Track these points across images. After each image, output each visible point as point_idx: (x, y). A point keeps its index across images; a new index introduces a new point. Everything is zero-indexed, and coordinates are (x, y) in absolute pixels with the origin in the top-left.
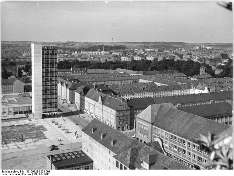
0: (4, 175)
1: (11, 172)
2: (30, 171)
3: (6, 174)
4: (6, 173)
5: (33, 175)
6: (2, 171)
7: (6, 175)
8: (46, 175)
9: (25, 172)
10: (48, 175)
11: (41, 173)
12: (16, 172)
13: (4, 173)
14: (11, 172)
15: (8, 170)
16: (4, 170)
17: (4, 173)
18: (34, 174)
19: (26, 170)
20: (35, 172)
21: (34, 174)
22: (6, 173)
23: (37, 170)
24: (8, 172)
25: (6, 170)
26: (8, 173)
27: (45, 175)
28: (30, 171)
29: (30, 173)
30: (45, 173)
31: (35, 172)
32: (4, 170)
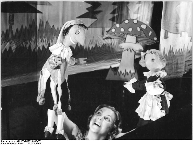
0: (4, 144)
3: (5, 144)
4: (5, 143)
5: (28, 144)
6: (2, 141)
8: (38, 144)
9: (20, 141)
10: (39, 144)
11: (34, 143)
12: (13, 142)
14: (9, 142)
17: (3, 143)
18: (28, 143)
19: (22, 140)
20: (29, 141)
21: (28, 143)
22: (5, 143)
23: (30, 140)
24: (7, 141)
27: (37, 144)
29: (25, 142)
31: (29, 141)
32: (3, 140)
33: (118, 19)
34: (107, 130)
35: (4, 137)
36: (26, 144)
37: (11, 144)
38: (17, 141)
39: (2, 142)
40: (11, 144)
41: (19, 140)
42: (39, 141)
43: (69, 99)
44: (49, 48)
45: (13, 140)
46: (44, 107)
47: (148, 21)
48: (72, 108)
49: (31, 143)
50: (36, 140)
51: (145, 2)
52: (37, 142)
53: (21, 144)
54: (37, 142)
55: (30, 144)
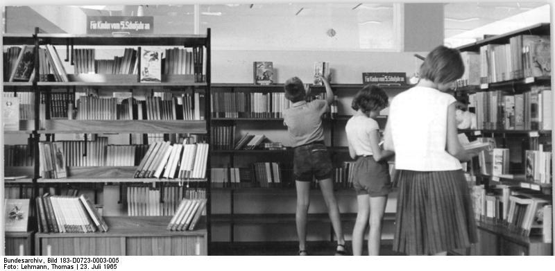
0: (11, 270)
1: (27, 261)
2: (71, 259)
3: (15, 267)
4: (13, 264)
6: (5, 260)
8: (110, 269)
9: (59, 260)
11: (96, 264)
12: (37, 261)
13: (10, 264)
14: (27, 261)
17: (10, 264)
19: (63, 257)
20: (84, 260)
21: (80, 267)
22: (13, 264)
24: (19, 261)
26: (19, 265)
27: (106, 270)
28: (71, 259)
31: (84, 260)
32: (9, 258)
37: (31, 267)
38: (49, 260)
39: (7, 263)
41: (55, 257)
42: (112, 260)
49: (90, 265)
50: (89, 257)
52: (108, 263)
54: (108, 263)
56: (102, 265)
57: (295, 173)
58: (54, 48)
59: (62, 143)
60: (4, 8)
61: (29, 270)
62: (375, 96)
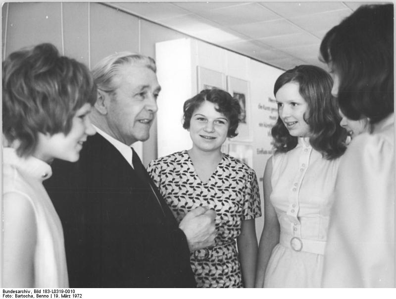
0: (8, 298)
1: (19, 292)
3: (11, 296)
4: (9, 294)
5: (53, 297)
6: (4, 291)
7: (10, 298)
9: (42, 291)
12: (27, 292)
13: (7, 294)
14: (19, 292)
15: (15, 289)
16: (6, 289)
17: (7, 294)
22: (9, 294)
24: (14, 292)
25: (10, 289)
26: (13, 295)
27: (74, 298)
30: (64, 293)
33: (180, 30)
34: (370, 6)
35: (390, 7)
36: (50, 298)
37: (24, 296)
38: (35, 291)
39: (5, 293)
40: (24, 296)
42: (68, 291)
43: (329, 50)
44: (302, 139)
45: (26, 289)
46: (375, 13)
47: (203, 244)
48: (327, 50)
51: (91, 3)
53: (41, 298)
54: (64, 293)
55: (77, 298)
56: (60, 294)
57: (331, 120)
58: (283, 70)
59: (144, 110)
60: (260, 110)
61: (43, 298)
62: (236, 240)
